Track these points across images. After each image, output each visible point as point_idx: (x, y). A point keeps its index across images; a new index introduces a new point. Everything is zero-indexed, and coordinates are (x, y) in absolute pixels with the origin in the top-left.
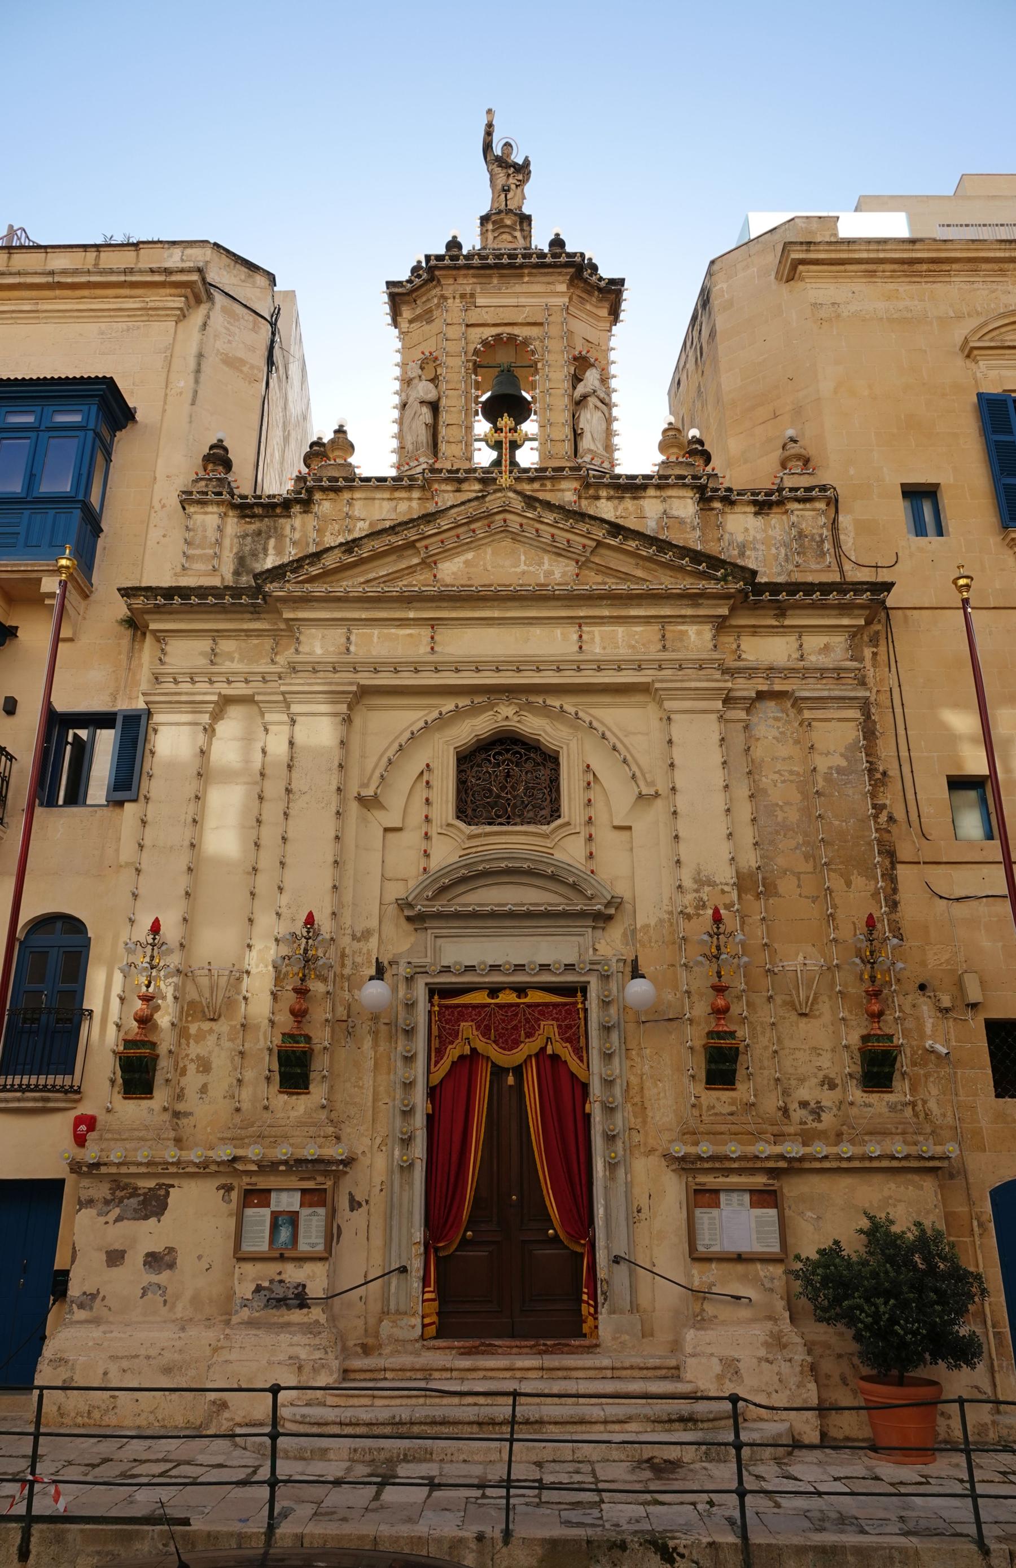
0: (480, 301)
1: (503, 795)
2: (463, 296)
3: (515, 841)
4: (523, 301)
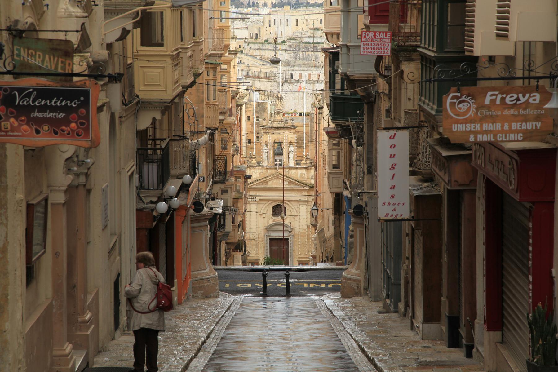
3: (278, 219)
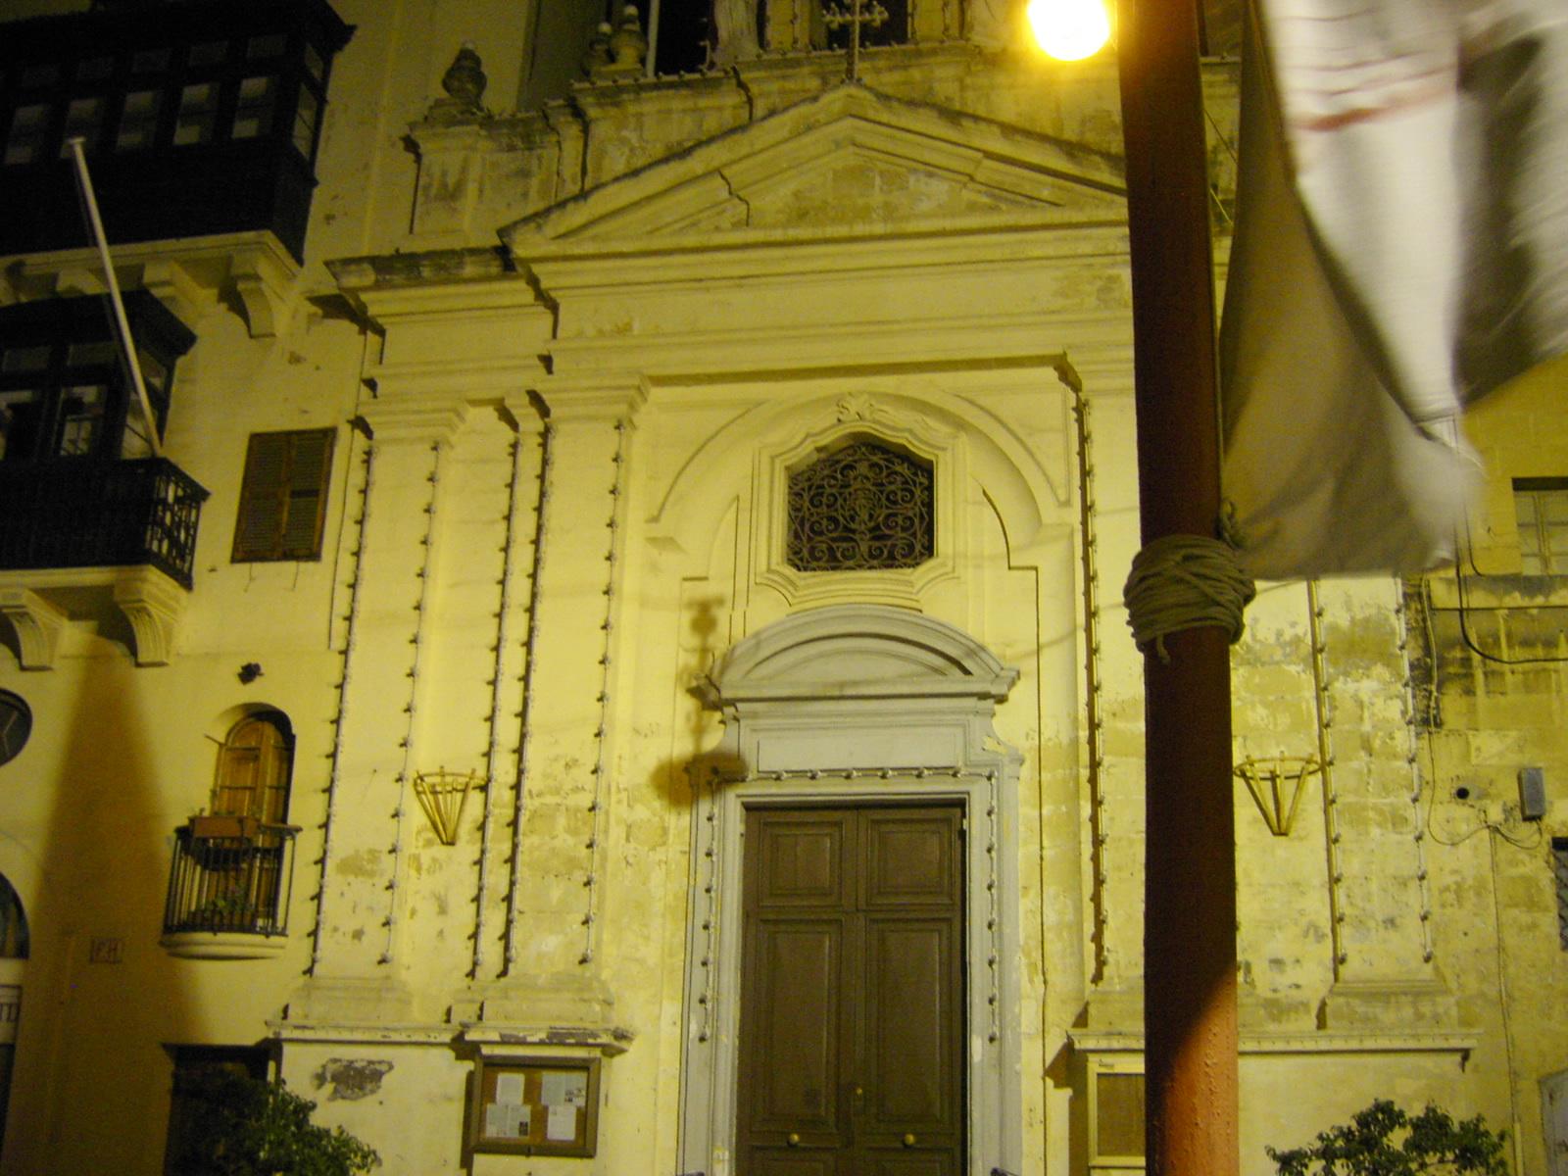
1: (853, 526)
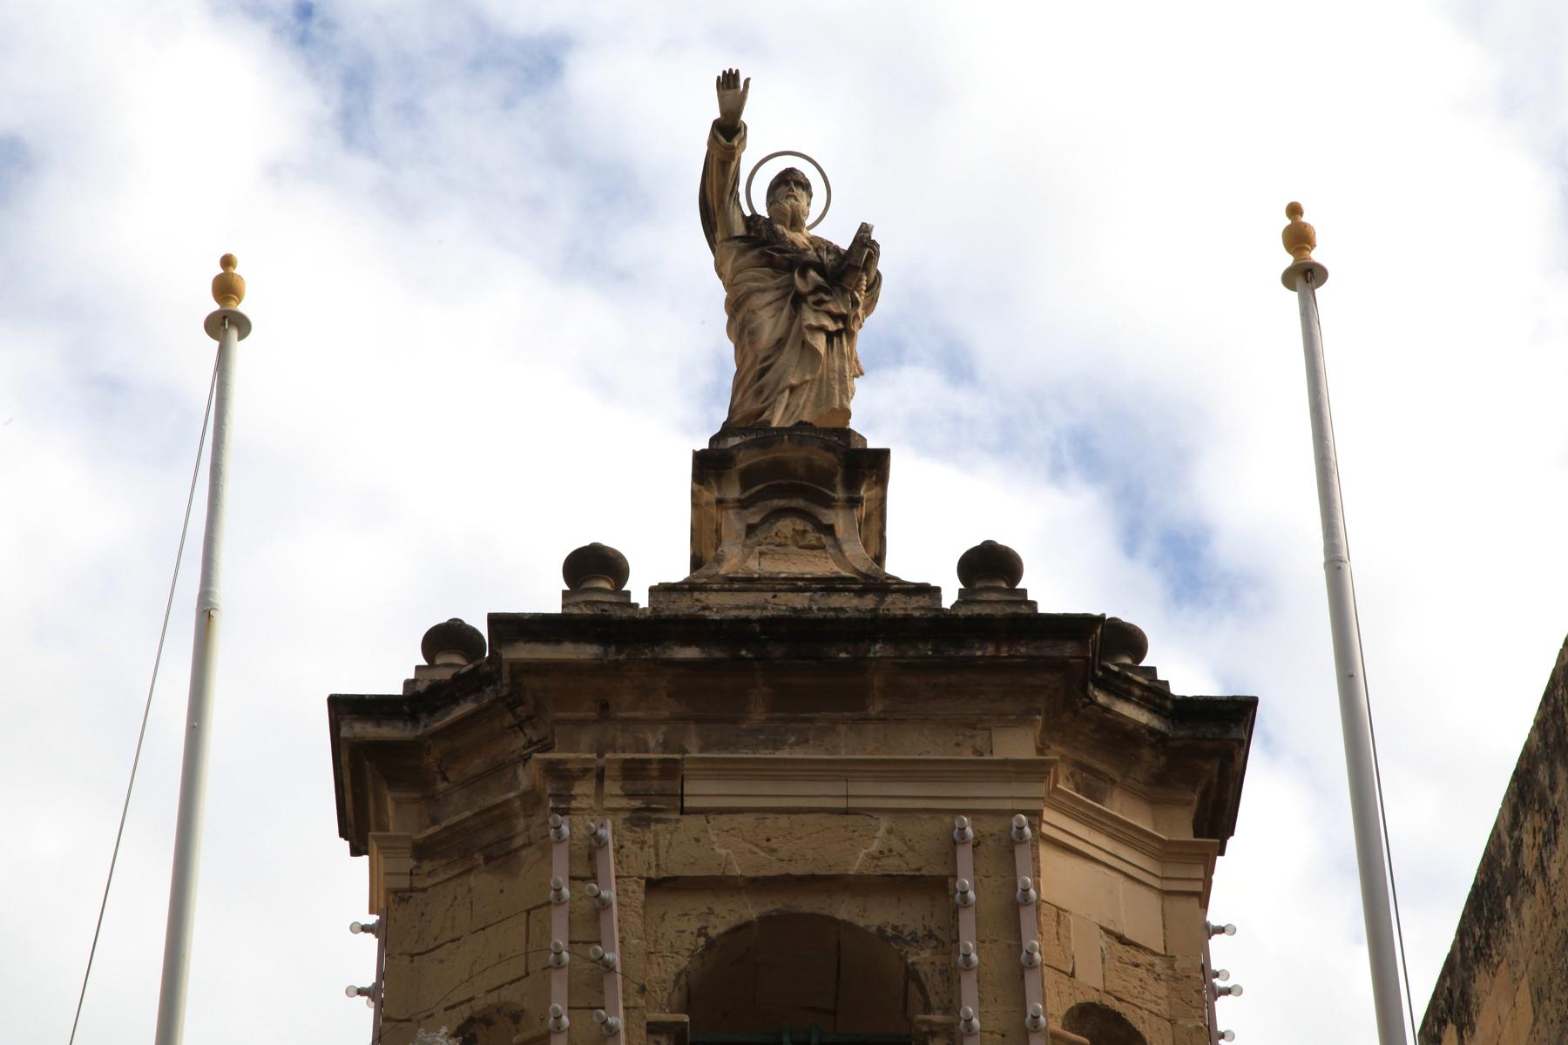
0: (699, 792)
2: (632, 771)
4: (866, 792)
